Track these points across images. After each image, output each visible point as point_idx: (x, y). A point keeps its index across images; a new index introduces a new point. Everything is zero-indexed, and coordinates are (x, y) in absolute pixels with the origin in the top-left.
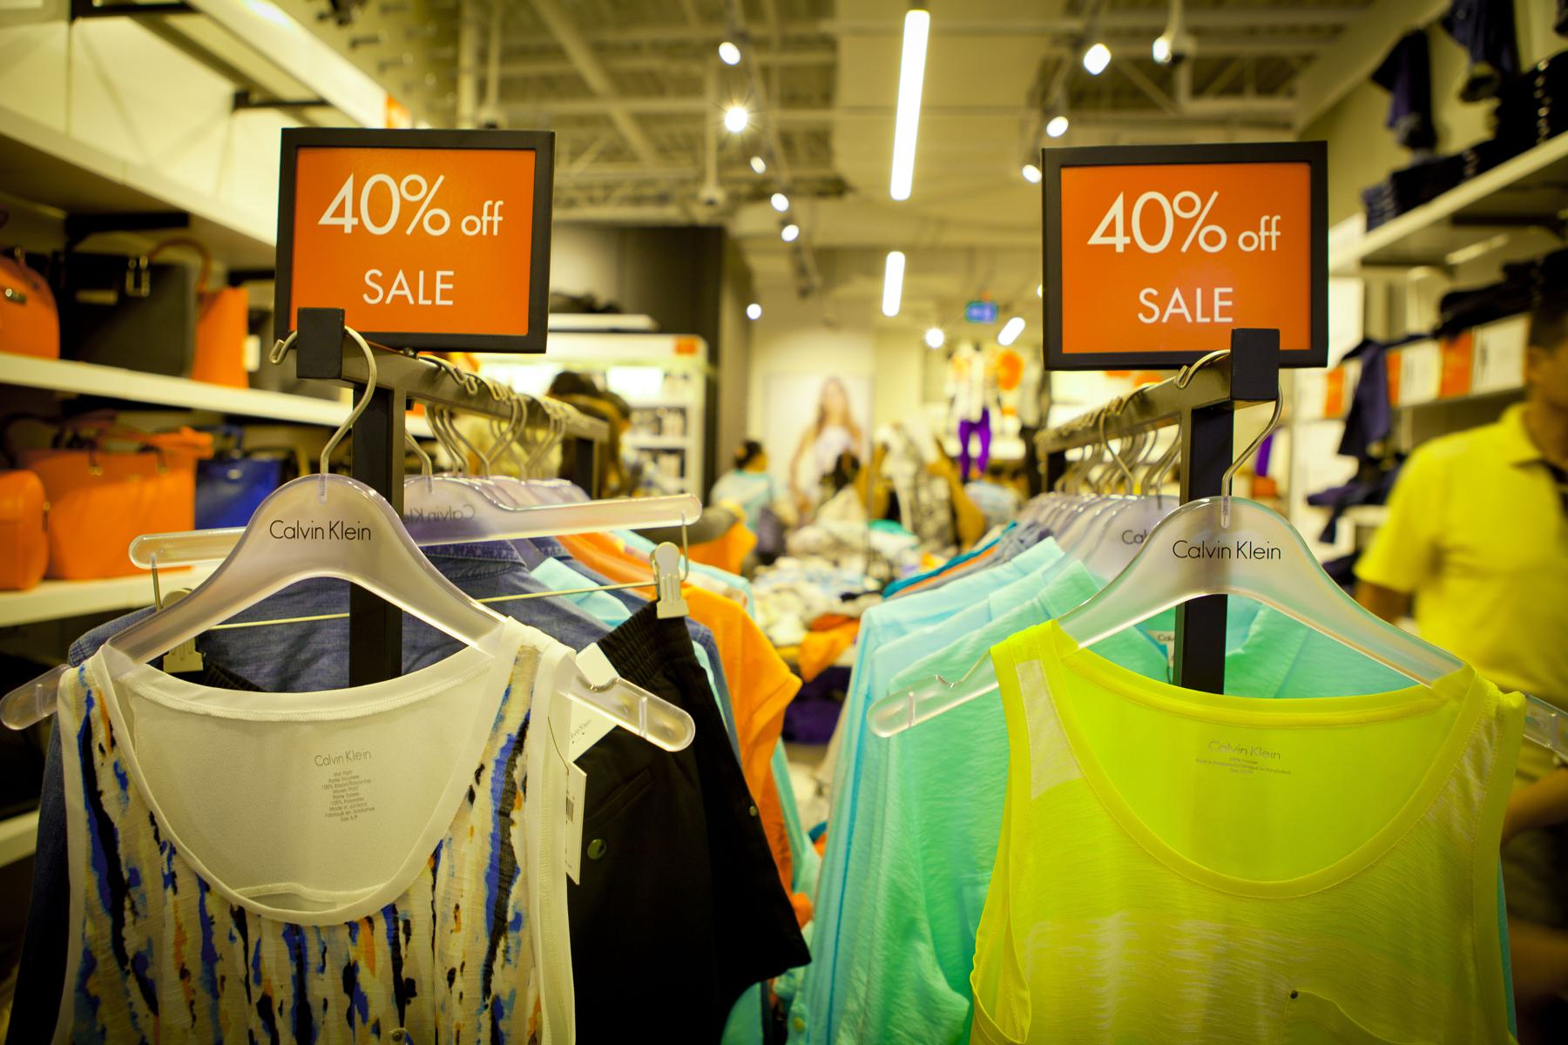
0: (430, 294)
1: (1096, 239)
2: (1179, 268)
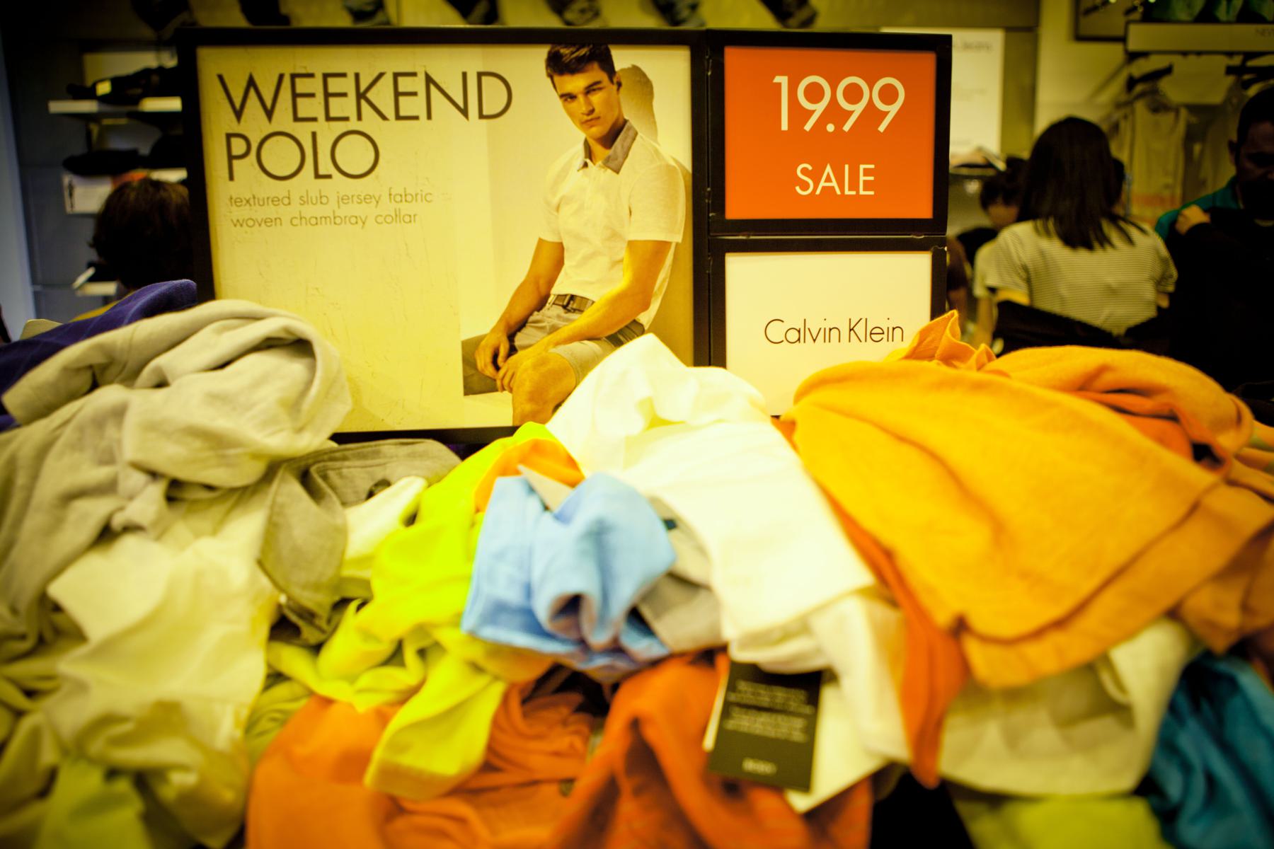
0: (854, 185)
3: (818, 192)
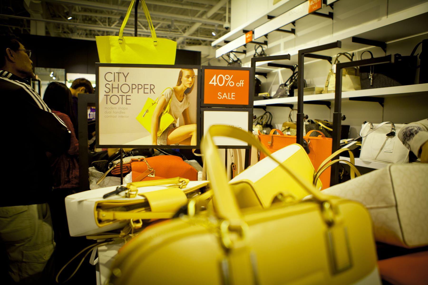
0: (230, 97)
1: (211, 83)
2: (226, 89)
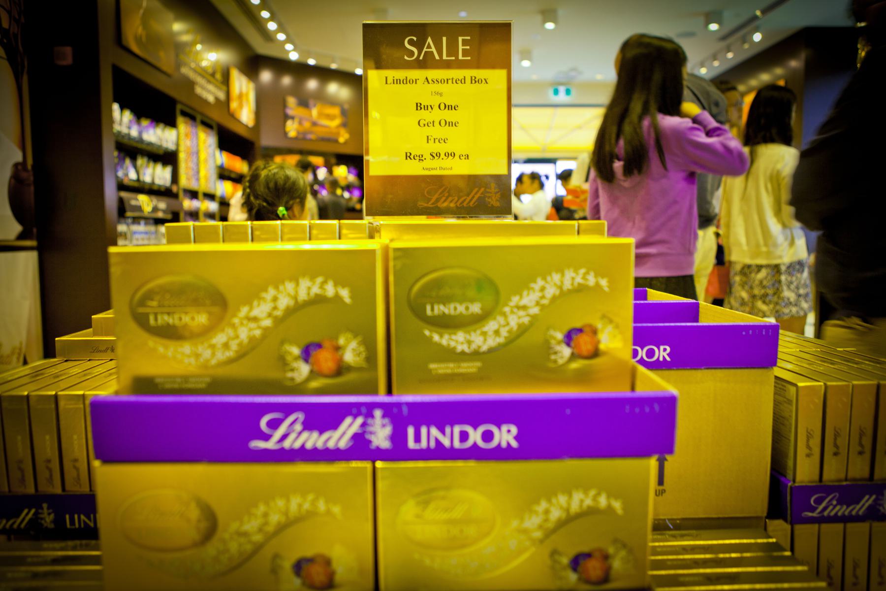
3: (421, 58)
